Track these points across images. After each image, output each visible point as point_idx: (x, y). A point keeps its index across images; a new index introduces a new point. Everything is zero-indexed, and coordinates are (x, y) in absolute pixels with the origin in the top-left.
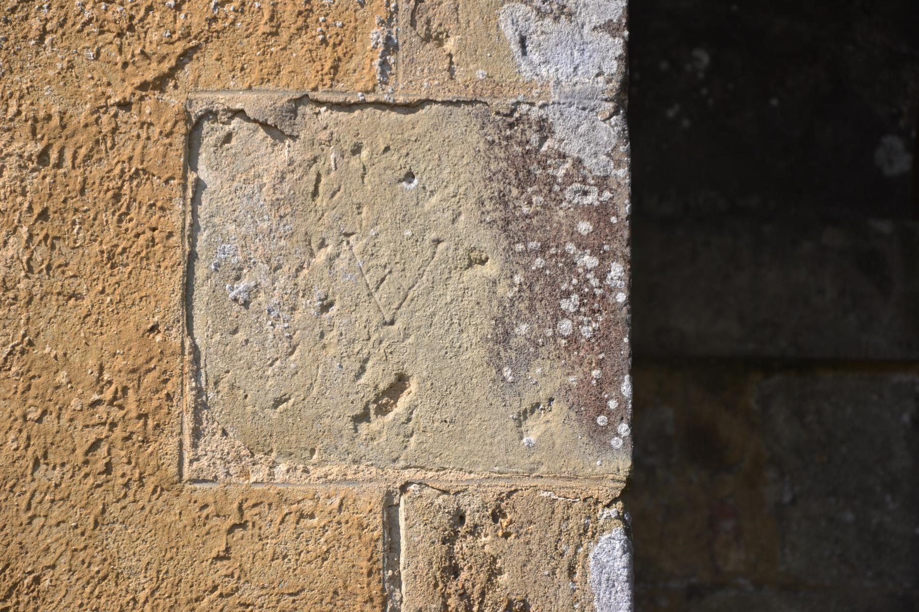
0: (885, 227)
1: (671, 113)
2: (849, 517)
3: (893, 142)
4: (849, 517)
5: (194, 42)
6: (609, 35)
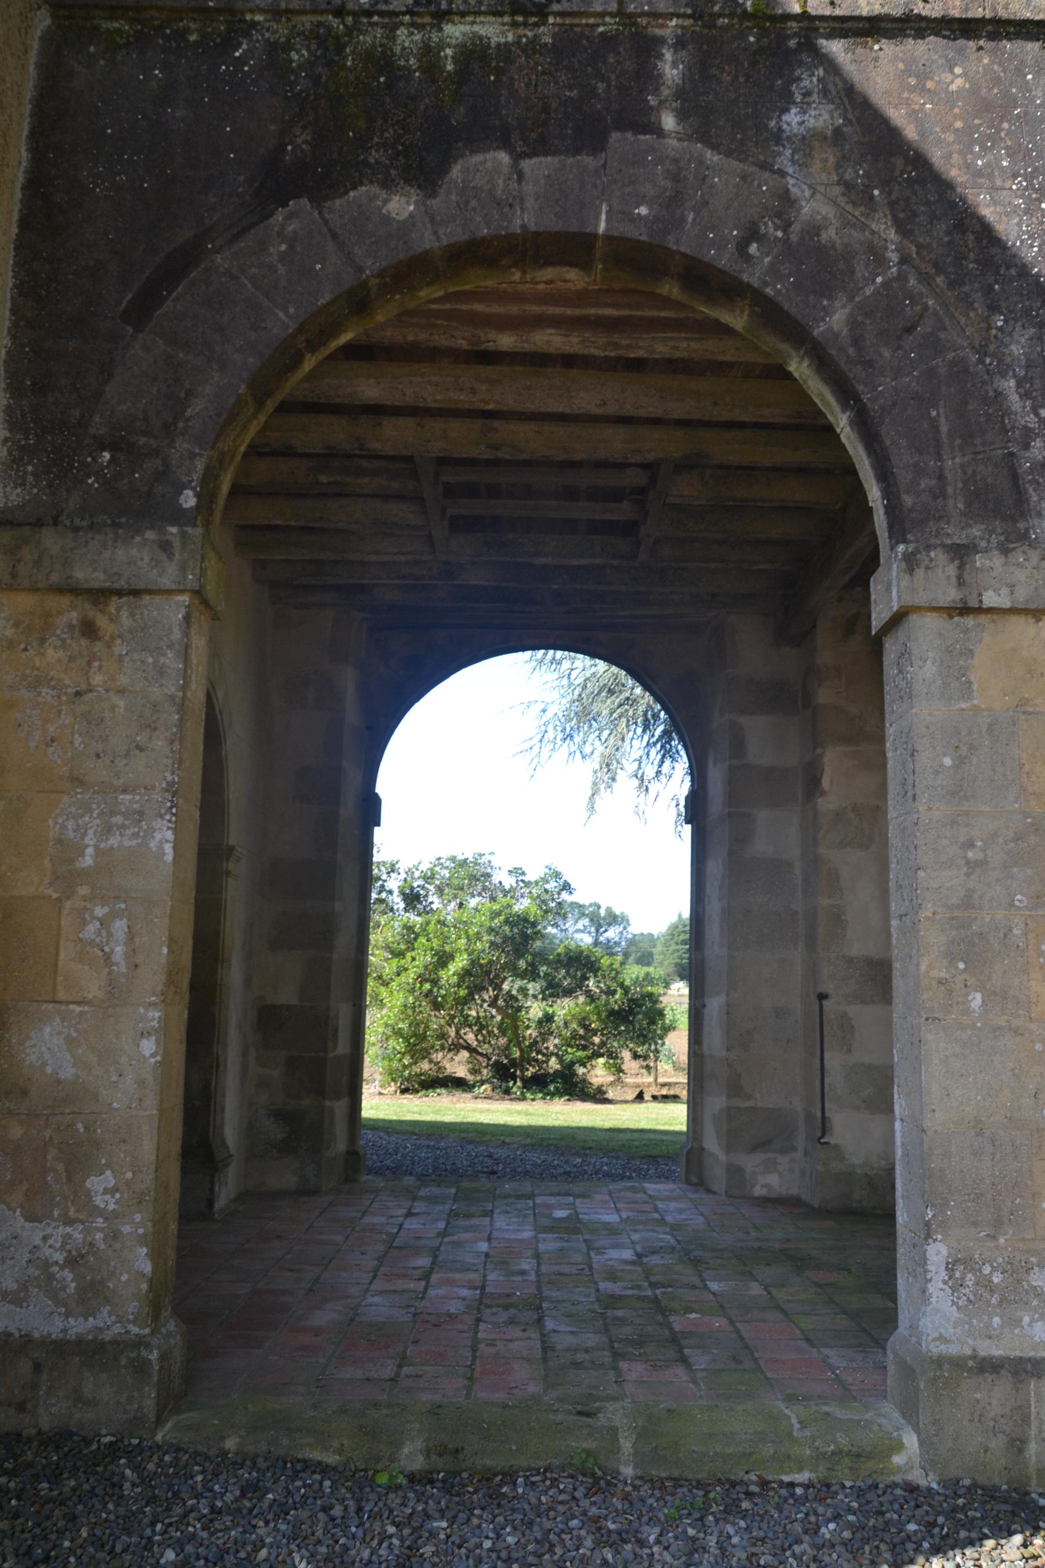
0: (174, 530)
1: (90, 481)
2: (150, 660)
3: (189, 493)
4: (150, 660)
5: (325, 481)
6: (987, 17)
